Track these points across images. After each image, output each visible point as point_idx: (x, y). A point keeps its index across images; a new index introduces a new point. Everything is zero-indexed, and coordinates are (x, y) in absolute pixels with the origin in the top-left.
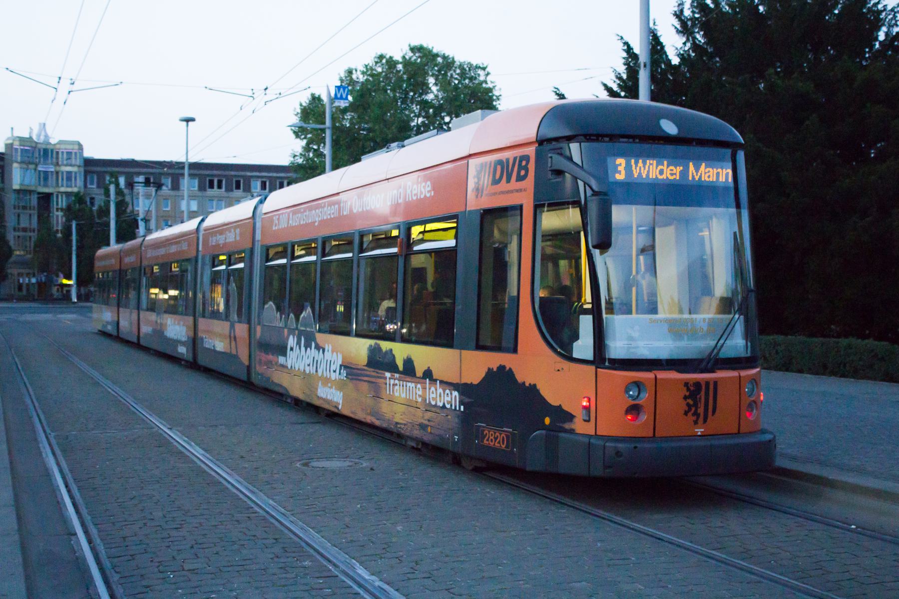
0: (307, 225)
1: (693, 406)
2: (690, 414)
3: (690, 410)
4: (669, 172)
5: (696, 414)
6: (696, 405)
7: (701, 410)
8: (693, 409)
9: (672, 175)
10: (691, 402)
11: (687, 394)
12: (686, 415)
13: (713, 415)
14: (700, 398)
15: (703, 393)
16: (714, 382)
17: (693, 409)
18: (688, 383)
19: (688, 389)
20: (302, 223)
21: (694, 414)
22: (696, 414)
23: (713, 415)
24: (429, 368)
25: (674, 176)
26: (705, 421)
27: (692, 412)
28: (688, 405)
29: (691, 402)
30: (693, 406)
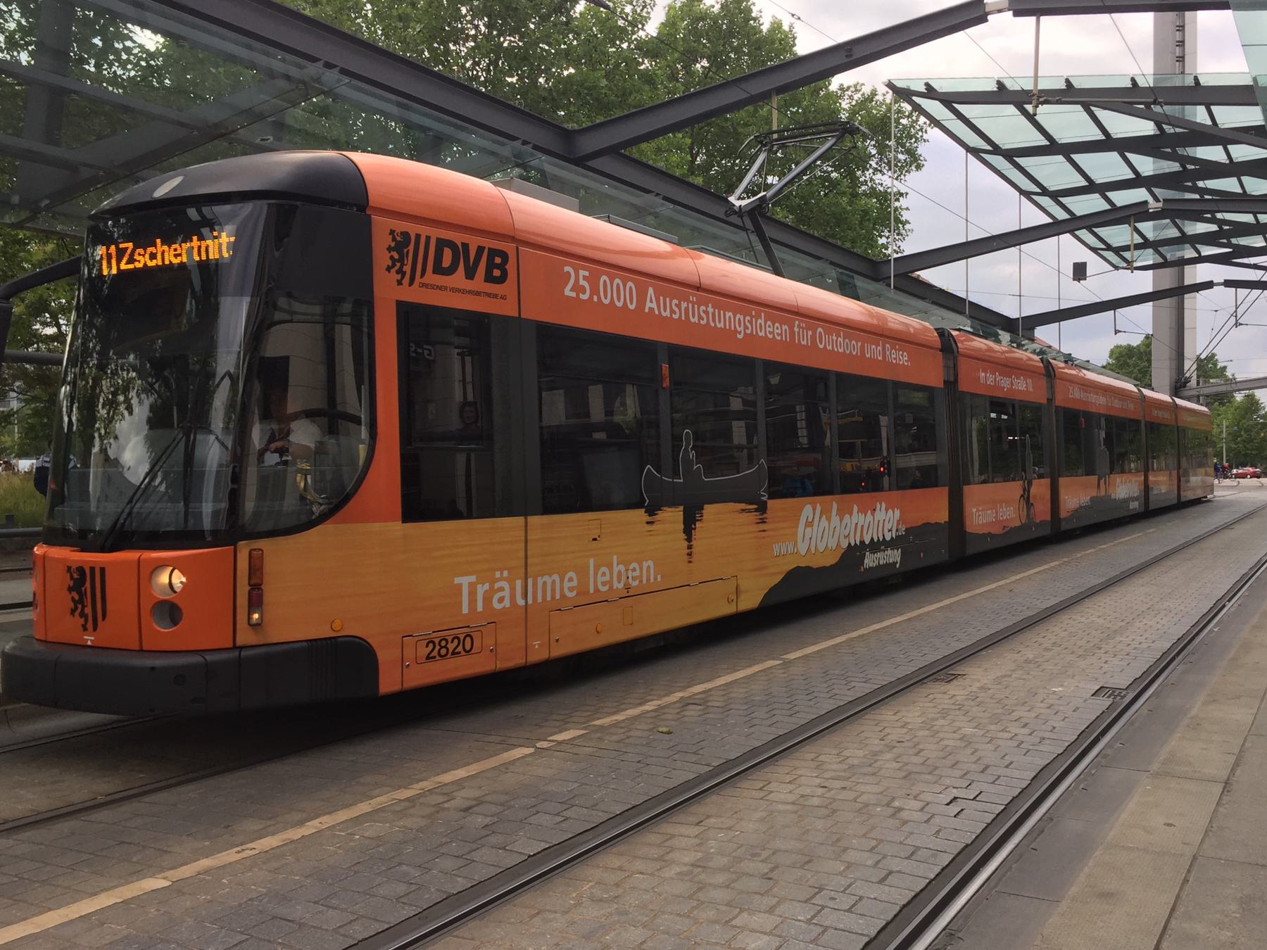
0: (886, 565)
1: (398, 261)
2: (393, 271)
3: (394, 265)
4: (172, 253)
5: (401, 272)
6: (401, 260)
7: (407, 269)
8: (398, 265)
9: (176, 256)
10: (396, 256)
11: (393, 244)
12: (389, 272)
13: (103, 620)
14: (408, 252)
15: (411, 247)
16: (91, 568)
17: (398, 265)
18: (394, 231)
19: (394, 239)
20: (881, 563)
21: (398, 272)
22: (400, 271)
23: (103, 620)
24: (773, 16)
25: (179, 258)
26: (95, 629)
27: (396, 268)
28: (392, 257)
29: (396, 256)
30: (398, 261)
